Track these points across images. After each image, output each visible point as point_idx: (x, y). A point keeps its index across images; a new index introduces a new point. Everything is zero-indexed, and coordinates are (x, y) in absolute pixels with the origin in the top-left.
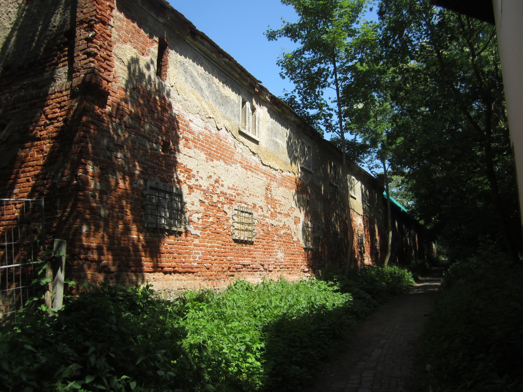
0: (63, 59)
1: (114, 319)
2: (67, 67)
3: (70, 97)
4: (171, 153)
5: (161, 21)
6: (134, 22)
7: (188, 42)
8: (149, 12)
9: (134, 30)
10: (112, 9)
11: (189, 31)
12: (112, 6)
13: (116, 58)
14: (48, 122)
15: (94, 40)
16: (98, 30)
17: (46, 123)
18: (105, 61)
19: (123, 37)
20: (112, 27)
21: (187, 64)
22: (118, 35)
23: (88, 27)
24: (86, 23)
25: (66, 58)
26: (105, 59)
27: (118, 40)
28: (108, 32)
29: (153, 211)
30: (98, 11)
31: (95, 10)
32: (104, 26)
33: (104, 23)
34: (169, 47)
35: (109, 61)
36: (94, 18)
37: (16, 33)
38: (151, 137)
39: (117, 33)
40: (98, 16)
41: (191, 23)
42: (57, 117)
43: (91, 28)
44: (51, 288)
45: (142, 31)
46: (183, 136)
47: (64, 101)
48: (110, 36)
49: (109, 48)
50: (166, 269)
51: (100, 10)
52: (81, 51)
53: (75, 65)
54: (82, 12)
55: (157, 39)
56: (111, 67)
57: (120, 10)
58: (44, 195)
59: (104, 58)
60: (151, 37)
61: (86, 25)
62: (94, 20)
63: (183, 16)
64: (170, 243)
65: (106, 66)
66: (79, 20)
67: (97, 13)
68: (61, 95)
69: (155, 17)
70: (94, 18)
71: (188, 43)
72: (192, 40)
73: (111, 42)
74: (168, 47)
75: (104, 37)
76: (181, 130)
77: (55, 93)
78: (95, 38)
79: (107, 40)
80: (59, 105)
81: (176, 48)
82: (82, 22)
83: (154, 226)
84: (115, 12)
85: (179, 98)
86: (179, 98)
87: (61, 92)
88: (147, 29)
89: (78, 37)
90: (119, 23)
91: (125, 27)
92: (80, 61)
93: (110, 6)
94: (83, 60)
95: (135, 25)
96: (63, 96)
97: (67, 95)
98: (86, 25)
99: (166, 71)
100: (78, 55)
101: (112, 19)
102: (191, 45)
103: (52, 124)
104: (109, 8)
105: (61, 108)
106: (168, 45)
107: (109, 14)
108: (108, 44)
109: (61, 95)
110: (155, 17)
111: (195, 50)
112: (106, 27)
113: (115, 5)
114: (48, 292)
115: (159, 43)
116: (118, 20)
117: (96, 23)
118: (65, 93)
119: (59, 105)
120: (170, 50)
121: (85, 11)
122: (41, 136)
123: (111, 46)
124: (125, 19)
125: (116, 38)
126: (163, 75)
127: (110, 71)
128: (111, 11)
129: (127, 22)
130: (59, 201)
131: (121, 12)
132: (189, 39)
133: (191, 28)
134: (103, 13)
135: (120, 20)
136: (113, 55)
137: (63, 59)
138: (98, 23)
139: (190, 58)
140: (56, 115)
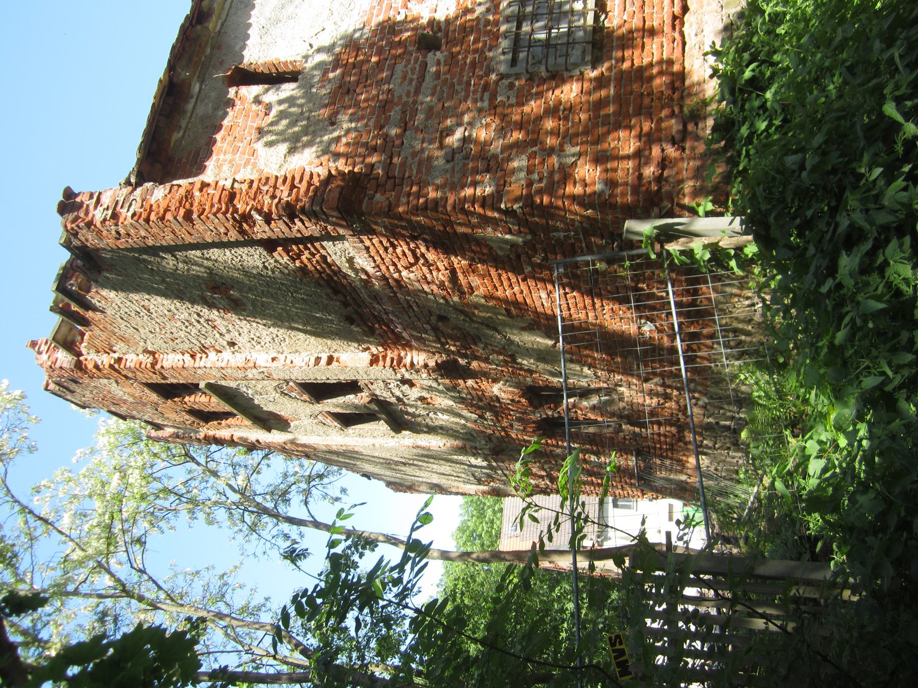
0: (312, 249)
1: (791, 160)
2: (325, 243)
3: (372, 235)
4: (440, 29)
5: (196, 88)
6: (215, 141)
7: (219, 24)
8: (189, 114)
9: (229, 139)
10: (204, 185)
11: (199, 27)
12: (198, 186)
13: (286, 166)
14: (422, 261)
15: (266, 209)
16: (247, 204)
17: (423, 265)
18: (296, 187)
19: (246, 157)
20: (234, 180)
21: (263, 21)
22: (245, 166)
23: (246, 222)
24: (241, 227)
25: (309, 245)
26: (293, 187)
27: (255, 165)
28: (245, 187)
29: (558, 52)
30: (214, 210)
31: (215, 214)
32: (238, 196)
33: (232, 196)
34: (241, 63)
35: (293, 178)
36: (229, 215)
37: (293, 325)
38: (415, 77)
39: (242, 170)
40: (223, 209)
41: (182, 26)
42: (410, 249)
43: (246, 217)
44: (713, 240)
45: (226, 123)
46: (402, 7)
47: (381, 242)
48: (252, 182)
49: (272, 182)
50: (677, 9)
51: (212, 206)
52: (290, 228)
53: (317, 234)
54: (226, 234)
55: (232, 91)
56: (303, 174)
57: (201, 169)
58: (546, 255)
59: (291, 190)
60: (231, 103)
61: (245, 225)
62: (232, 214)
63: (174, 47)
64: (622, 7)
65: (305, 183)
66: (240, 236)
67: (219, 210)
68: (372, 248)
69: (193, 100)
70: (229, 215)
71: (222, 25)
72: (214, 18)
73: (260, 180)
74: (241, 66)
75: (256, 193)
76: (391, 13)
77: (370, 256)
78: (262, 208)
79: (259, 188)
80: (390, 250)
81: (237, 48)
82: (242, 232)
83: (590, 47)
84: (208, 176)
85: (330, 27)
86: (330, 27)
87: (367, 249)
88: (221, 113)
89: (269, 234)
90: (225, 168)
91: (229, 157)
92: (307, 228)
93: (201, 190)
94: (304, 224)
95: (218, 137)
96: (373, 244)
97: (371, 240)
98: (245, 225)
99: (285, 63)
100: (299, 231)
101: (221, 184)
102: (224, 17)
103: (423, 255)
104: (205, 190)
105: (394, 247)
106: (237, 68)
107: (215, 189)
108: (266, 184)
109: (372, 248)
110: (193, 100)
111: (230, 7)
112: (238, 192)
113: (197, 180)
114: (721, 244)
115: (238, 86)
116: (220, 170)
117: (236, 210)
118: (368, 243)
119: (390, 250)
120: (246, 61)
121: (222, 230)
122: (446, 269)
123: (268, 179)
124: (214, 157)
125: (252, 170)
126: (295, 66)
127: (312, 175)
128: (208, 185)
129: (218, 154)
130: (555, 234)
131: (205, 167)
132: (213, 25)
133: (191, 24)
134: (216, 200)
135: (219, 167)
136: (283, 173)
137: (312, 249)
138: (234, 206)
139: (249, 17)
140: (407, 251)
